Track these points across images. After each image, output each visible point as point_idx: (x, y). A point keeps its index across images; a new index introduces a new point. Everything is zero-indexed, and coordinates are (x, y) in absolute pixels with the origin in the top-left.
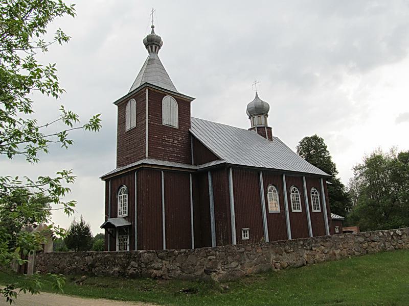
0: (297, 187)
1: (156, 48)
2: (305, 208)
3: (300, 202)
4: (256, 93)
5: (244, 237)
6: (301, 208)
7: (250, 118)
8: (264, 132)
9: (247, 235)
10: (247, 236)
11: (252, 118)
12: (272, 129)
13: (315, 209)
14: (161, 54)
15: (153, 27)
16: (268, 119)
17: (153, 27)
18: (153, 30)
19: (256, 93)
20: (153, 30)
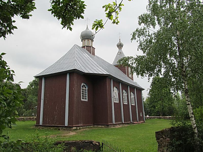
0: (81, 86)
1: (121, 47)
2: (120, 100)
3: (81, 94)
4: (87, 26)
5: (82, 99)
6: (87, 99)
7: (82, 41)
8: (90, 49)
9: (86, 98)
10: (86, 99)
11: (83, 41)
12: (95, 49)
13: (132, 104)
14: (123, 49)
15: (120, 39)
16: (93, 43)
17: (120, 39)
18: (120, 40)
19: (87, 26)
20: (120, 40)
